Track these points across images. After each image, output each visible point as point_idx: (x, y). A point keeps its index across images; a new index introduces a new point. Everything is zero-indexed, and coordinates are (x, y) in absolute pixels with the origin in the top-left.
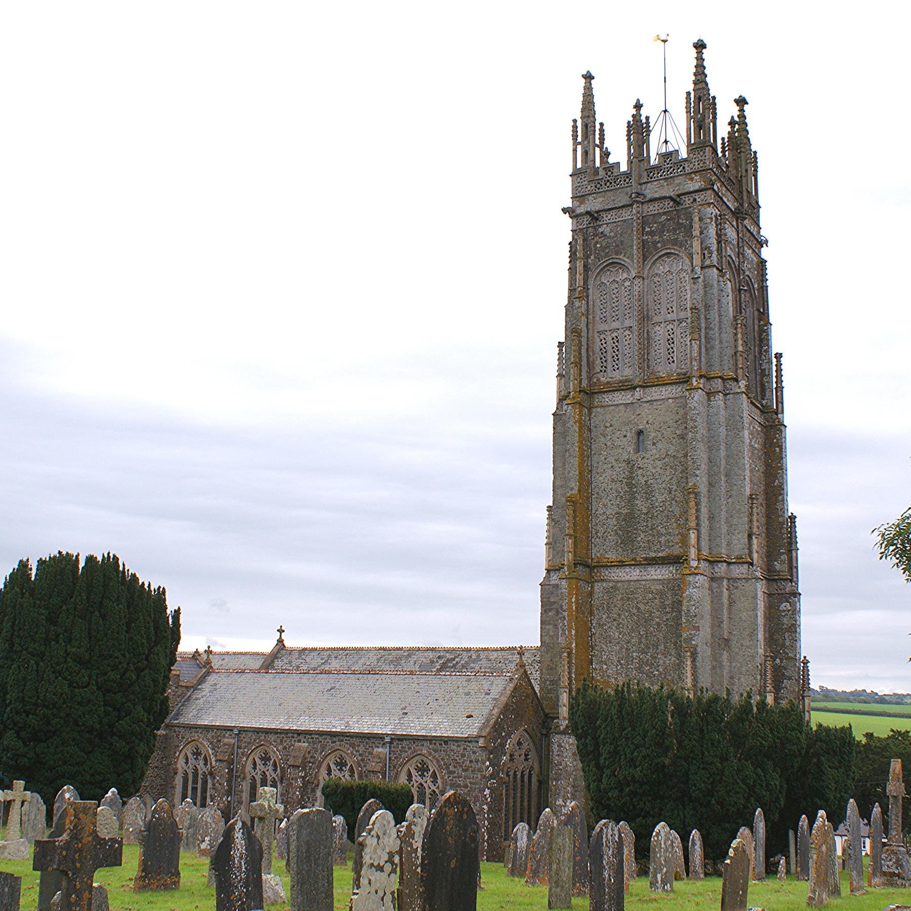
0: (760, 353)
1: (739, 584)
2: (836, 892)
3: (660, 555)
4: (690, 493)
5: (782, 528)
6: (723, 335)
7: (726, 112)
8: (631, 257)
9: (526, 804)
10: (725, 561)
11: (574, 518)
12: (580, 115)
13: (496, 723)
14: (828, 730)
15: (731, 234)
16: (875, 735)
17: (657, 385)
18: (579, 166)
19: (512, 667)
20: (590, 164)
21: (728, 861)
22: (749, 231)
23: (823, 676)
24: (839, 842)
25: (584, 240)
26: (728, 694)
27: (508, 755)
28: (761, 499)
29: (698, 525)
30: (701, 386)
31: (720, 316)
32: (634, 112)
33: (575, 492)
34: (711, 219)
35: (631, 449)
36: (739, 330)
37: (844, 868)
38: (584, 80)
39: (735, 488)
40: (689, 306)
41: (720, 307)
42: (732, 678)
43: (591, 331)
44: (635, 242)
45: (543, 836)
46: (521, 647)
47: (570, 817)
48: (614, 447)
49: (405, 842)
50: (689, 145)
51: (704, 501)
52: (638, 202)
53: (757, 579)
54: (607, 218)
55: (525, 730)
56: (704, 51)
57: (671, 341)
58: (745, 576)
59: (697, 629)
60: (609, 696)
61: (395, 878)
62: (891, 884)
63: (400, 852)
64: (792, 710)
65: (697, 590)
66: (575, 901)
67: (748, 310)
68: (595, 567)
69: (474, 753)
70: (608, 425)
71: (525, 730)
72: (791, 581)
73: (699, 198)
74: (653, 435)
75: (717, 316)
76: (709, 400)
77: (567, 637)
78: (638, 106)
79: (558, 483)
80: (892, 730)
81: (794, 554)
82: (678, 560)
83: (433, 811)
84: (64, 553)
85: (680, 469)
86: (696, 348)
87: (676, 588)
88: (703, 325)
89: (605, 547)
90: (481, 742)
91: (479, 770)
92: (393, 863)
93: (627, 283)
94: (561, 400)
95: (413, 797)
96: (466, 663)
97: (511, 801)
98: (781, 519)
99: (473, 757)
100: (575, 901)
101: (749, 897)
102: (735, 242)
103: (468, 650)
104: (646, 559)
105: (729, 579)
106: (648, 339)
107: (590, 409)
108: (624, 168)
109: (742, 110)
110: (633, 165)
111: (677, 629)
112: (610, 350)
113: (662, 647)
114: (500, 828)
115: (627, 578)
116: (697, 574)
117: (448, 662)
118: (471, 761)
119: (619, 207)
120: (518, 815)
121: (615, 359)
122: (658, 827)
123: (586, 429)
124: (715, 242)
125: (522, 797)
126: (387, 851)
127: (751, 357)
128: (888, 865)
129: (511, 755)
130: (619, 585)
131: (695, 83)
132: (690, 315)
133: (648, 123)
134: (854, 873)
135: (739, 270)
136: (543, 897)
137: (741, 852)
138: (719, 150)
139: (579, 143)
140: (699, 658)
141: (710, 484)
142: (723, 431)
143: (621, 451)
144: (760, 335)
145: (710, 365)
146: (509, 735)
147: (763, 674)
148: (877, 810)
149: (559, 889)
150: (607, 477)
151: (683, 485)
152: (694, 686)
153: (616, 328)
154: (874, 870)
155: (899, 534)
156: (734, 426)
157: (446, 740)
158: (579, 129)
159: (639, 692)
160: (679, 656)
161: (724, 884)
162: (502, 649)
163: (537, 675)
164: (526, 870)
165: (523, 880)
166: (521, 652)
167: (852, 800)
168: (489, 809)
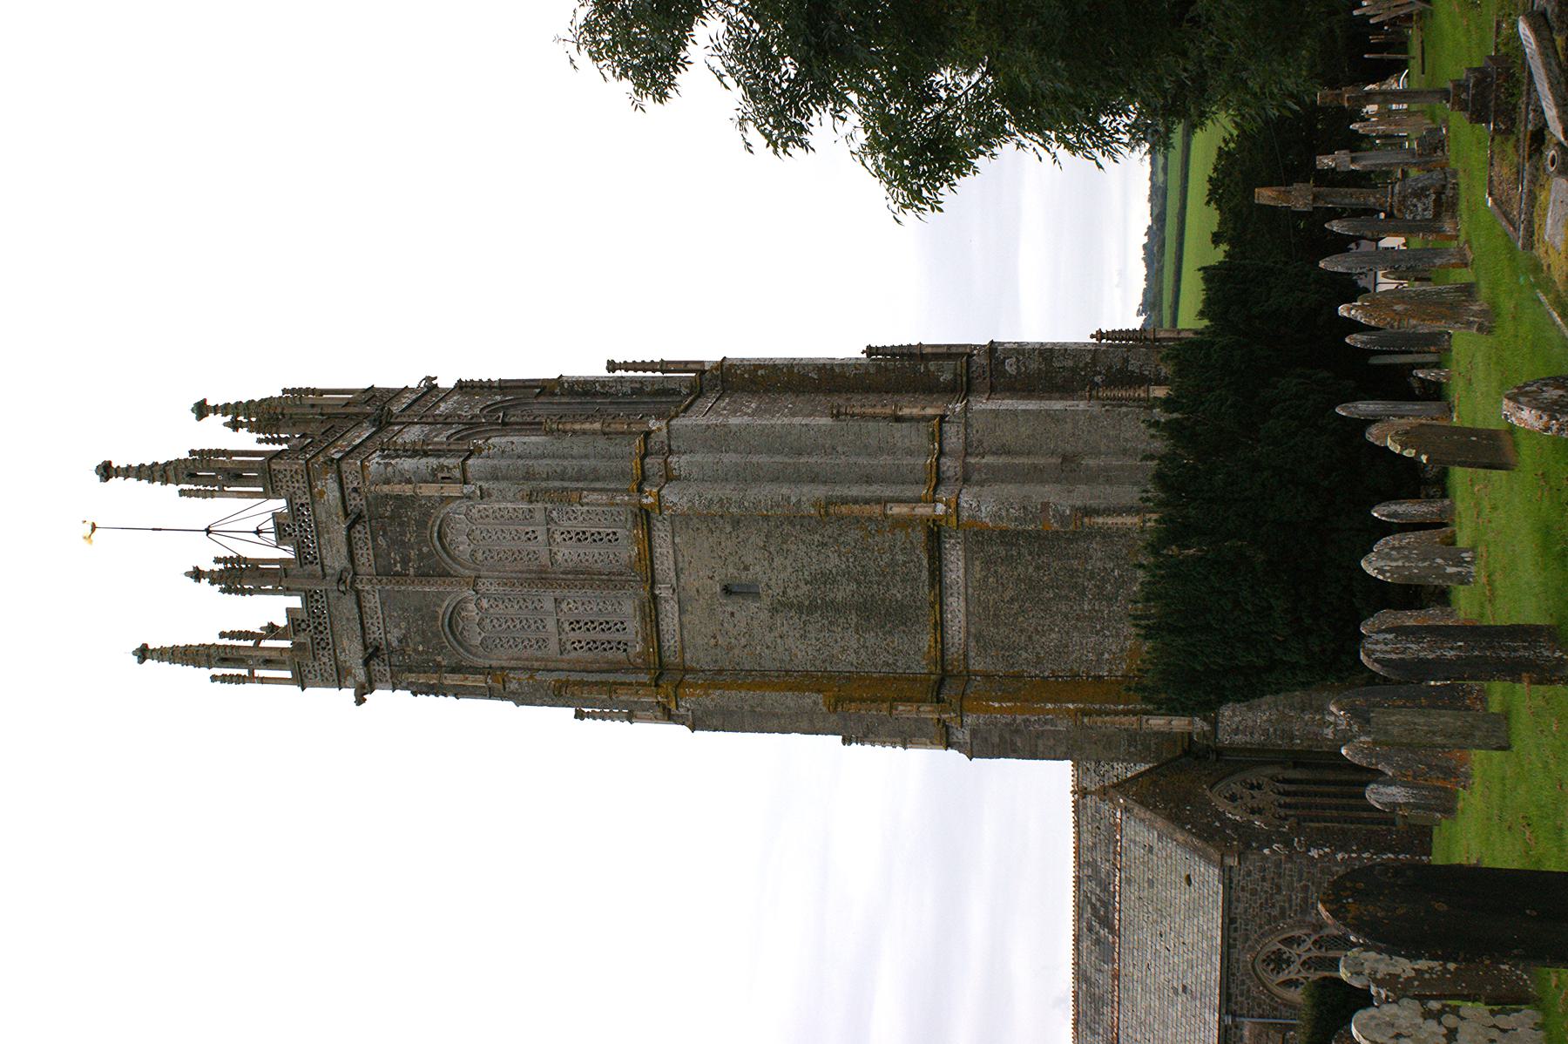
0: (605, 395)
1: (974, 436)
2: (1468, 290)
3: (925, 562)
4: (827, 513)
7: (217, 435)
8: (441, 596)
9: (1332, 789)
10: (938, 459)
11: (863, 700)
12: (204, 670)
13: (1199, 837)
14: (1208, 302)
15: (413, 434)
16: (1215, 229)
17: (652, 561)
19: (1106, 807)
20: (286, 656)
21: (1424, 458)
22: (410, 406)
23: (1123, 312)
26: (1151, 457)
27: (1252, 817)
28: (838, 400)
29: (878, 501)
31: (543, 456)
33: (820, 698)
34: (387, 465)
35: (753, 606)
36: (568, 427)
37: (1429, 280)
38: (148, 661)
39: (820, 441)
40: (525, 506)
41: (529, 456)
42: (1125, 452)
43: (560, 666)
45: (1387, 759)
46: (1074, 792)
47: (1354, 713)
48: (749, 632)
49: (1404, 989)
50: (265, 495)
51: (840, 491)
52: (353, 582)
53: (966, 409)
54: (376, 633)
55: (1211, 788)
56: (114, 465)
57: (581, 537)
59: (1045, 505)
61: (1467, 1008)
62: (1453, 206)
63: (1422, 999)
64: (1177, 357)
65: (981, 504)
66: (1495, 706)
67: (536, 412)
68: (943, 669)
69: (1249, 873)
70: (713, 642)
71: (1211, 788)
72: (970, 356)
73: (352, 482)
74: (731, 570)
75: (545, 461)
76: (678, 478)
77: (1058, 716)
78: (197, 575)
79: (805, 724)
80: (1208, 203)
81: (929, 350)
82: (935, 534)
83: (1352, 938)
84: (837, 135)
85: (787, 528)
86: (594, 497)
87: (979, 538)
88: (557, 484)
89: (912, 651)
90: (1232, 861)
91: (1278, 865)
92: (1441, 1012)
93: (485, 603)
94: (669, 717)
95: (1325, 978)
96: (1099, 884)
97: (1327, 813)
100: (1495, 706)
101: (1480, 425)
102: (427, 429)
103: (1078, 881)
104: (932, 586)
105: (967, 454)
106: (577, 573)
107: (686, 671)
108: (296, 602)
109: (216, 409)
110: (292, 586)
111: (1045, 538)
112: (592, 635)
114: (1374, 832)
115: (961, 616)
116: (958, 504)
117: (1097, 916)
118: (1264, 879)
120: (1352, 802)
121: (606, 626)
123: (719, 678)
124: (424, 460)
125: (1322, 795)
126: (1420, 1020)
127: (611, 409)
128: (1423, 209)
129: (1253, 812)
131: (166, 481)
132: (540, 505)
133: (225, 560)
134: (1438, 261)
135: (472, 425)
136: (1490, 759)
137: (1407, 438)
138: (278, 447)
139: (251, 672)
140: (1094, 503)
141: (813, 481)
142: (729, 458)
143: (755, 623)
144: (577, 394)
145: (623, 475)
146: (1219, 816)
147: (1120, 402)
148: (1336, 226)
149: (1477, 733)
150: (799, 646)
151: (813, 523)
152: (1138, 511)
153: (554, 622)
154: (1431, 232)
155: (903, 182)
156: (719, 439)
157: (1229, 921)
158: (228, 671)
159: (1148, 600)
160: (1090, 535)
161: (1463, 464)
162: (1077, 824)
163: (1119, 767)
164: (1444, 789)
165: (1462, 793)
166: (1080, 792)
167: (1322, 264)
168: (1342, 849)
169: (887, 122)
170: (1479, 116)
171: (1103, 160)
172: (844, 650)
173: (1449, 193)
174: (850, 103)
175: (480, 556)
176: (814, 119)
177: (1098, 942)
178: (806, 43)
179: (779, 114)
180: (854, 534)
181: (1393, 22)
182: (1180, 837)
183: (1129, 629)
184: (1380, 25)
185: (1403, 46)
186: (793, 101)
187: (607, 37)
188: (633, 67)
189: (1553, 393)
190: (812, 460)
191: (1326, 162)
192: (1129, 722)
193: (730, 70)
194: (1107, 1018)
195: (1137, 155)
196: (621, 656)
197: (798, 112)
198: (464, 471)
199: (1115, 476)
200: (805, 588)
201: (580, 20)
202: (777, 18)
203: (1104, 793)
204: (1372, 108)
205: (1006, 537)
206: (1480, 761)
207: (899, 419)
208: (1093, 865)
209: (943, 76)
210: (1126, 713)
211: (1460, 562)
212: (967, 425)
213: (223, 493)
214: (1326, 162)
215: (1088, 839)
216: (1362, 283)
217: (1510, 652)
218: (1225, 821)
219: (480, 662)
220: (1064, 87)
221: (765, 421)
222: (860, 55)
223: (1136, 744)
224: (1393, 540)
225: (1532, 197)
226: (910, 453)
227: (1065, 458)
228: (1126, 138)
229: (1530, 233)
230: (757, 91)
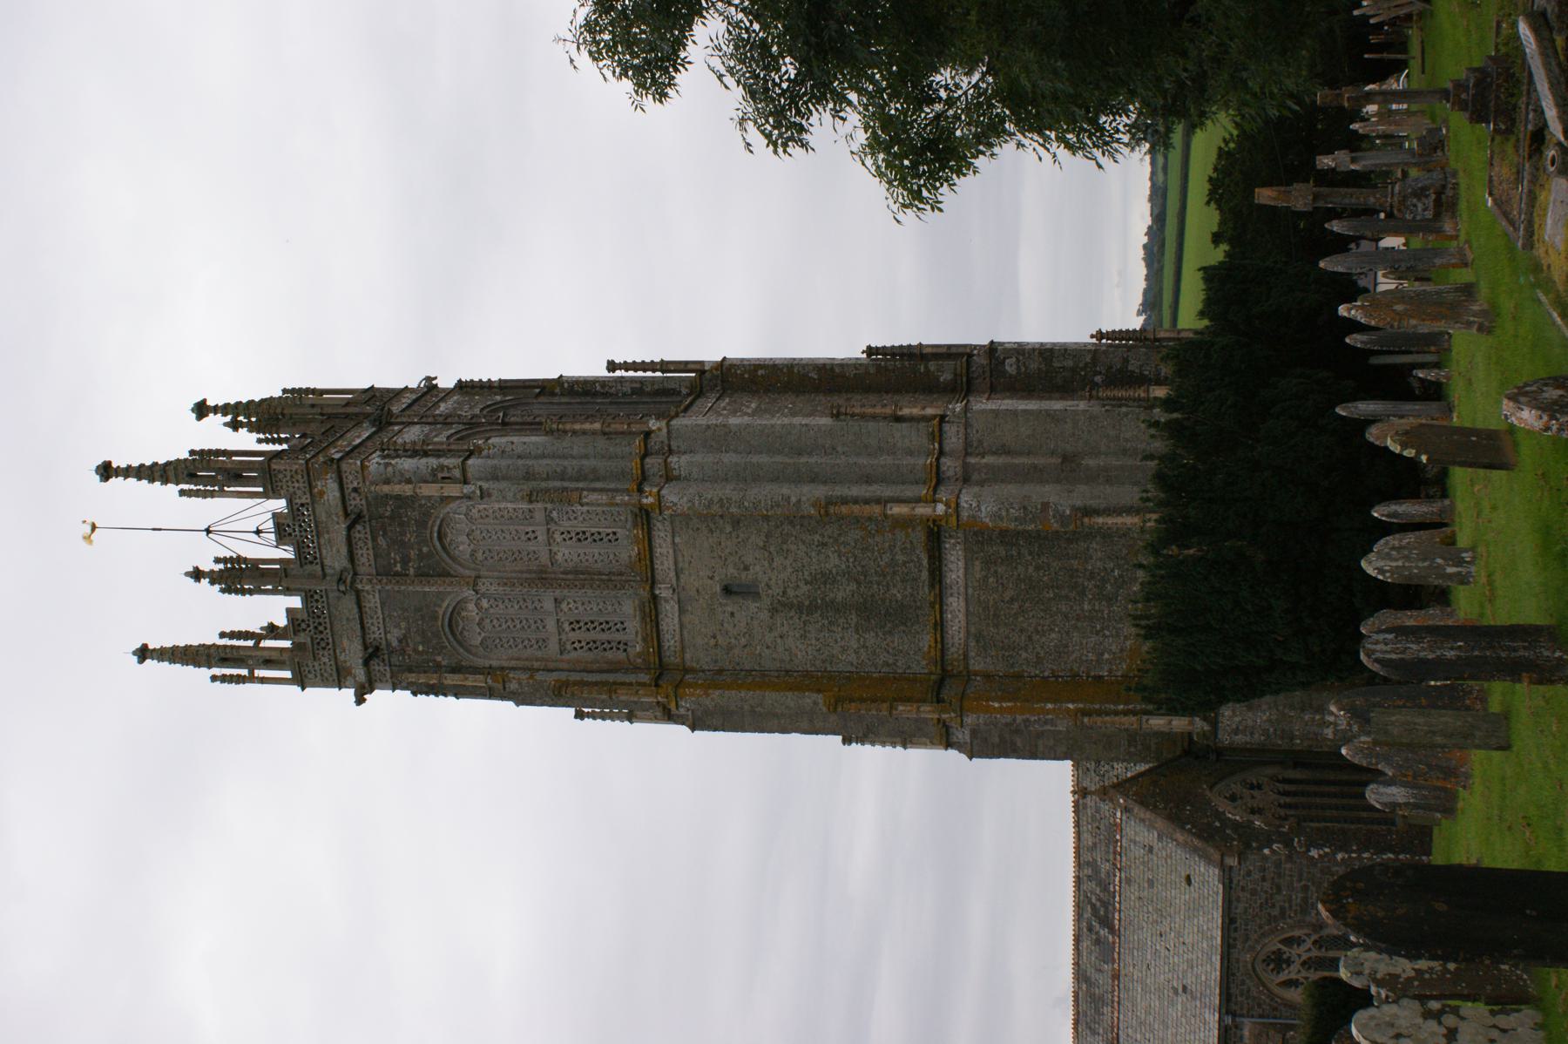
0: (605, 395)
2: (1468, 290)
4: (827, 514)
5: (886, 369)
6: (575, 452)
7: (217, 435)
8: (441, 596)
9: (1332, 789)
10: (938, 459)
11: (862, 700)
12: (203, 670)
13: (1199, 836)
14: (1208, 302)
15: (413, 434)
17: (652, 562)
19: (1105, 807)
20: (285, 656)
21: (1424, 458)
22: (410, 406)
23: (1123, 312)
24: (1386, 284)
25: (410, 670)
26: (1150, 457)
27: (1252, 817)
28: (838, 400)
29: (878, 501)
30: (655, 490)
31: (543, 456)
32: (205, 582)
33: (820, 698)
34: (387, 465)
36: (568, 427)
37: (1428, 279)
38: (148, 661)
40: (525, 506)
42: (1125, 452)
43: (561, 666)
44: (418, 589)
46: (1074, 792)
47: (1360, 716)
50: (266, 495)
51: (840, 491)
52: (353, 581)
53: (966, 409)
54: (376, 633)
55: (1211, 788)
56: (114, 465)
57: (581, 537)
58: (962, 430)
59: (1045, 506)
60: (1155, 650)
61: (1467, 1008)
63: (1422, 999)
64: (1177, 356)
65: (981, 504)
66: (1495, 706)
67: (536, 412)
68: (943, 669)
69: (1249, 873)
70: (712, 642)
71: (1211, 788)
72: (970, 356)
73: (352, 482)
75: (545, 462)
76: (678, 478)
78: (197, 575)
82: (935, 535)
83: (1352, 938)
84: (838, 134)
85: (787, 528)
86: (593, 497)
87: (978, 537)
88: (558, 484)
89: (912, 651)
90: (1232, 861)
91: (1278, 865)
93: (485, 603)
94: (669, 716)
95: (1325, 978)
97: (1328, 813)
98: (872, 370)
99: (1257, 876)
100: (1495, 706)
101: (1480, 425)
102: (427, 429)
103: (1078, 881)
104: (932, 586)
106: (576, 572)
107: (687, 671)
108: (296, 602)
109: (216, 410)
110: (292, 586)
112: (593, 635)
113: (1075, 563)
115: (961, 616)
116: (958, 504)
117: (1097, 916)
118: (1264, 879)
119: (360, 607)
120: (1352, 802)
121: (606, 626)
122: (1371, 571)
123: (719, 678)
124: (424, 460)
126: (1420, 1020)
128: (1423, 209)
129: (1253, 812)
130: (973, 630)
131: (165, 481)
132: (540, 505)
133: (224, 560)
134: (1438, 261)
135: (472, 425)
137: (1407, 438)
138: (278, 447)
139: (251, 672)
140: (1093, 503)
141: (813, 481)
142: (729, 458)
143: (755, 622)
144: (577, 394)
146: (1219, 815)
147: (1120, 402)
148: (1336, 226)
149: (1477, 733)
150: (798, 646)
154: (1431, 232)
155: (903, 182)
156: (720, 439)
157: (1229, 922)
158: (228, 671)
159: (1148, 600)
160: (1090, 535)
162: (1077, 824)
163: (1119, 768)
164: (1444, 789)
165: (1462, 793)
166: (1081, 792)
167: (1322, 264)
168: (1341, 849)
169: (887, 122)
170: (1478, 116)
171: (1103, 161)
173: (1450, 193)
174: (850, 103)
175: (480, 556)
176: (814, 119)
177: (1098, 942)
178: (806, 43)
179: (779, 114)
180: (855, 534)
181: (1393, 22)
182: (1180, 837)
183: (1129, 629)
184: (1380, 25)
185: (1403, 46)
187: (607, 37)
188: (633, 67)
189: (1553, 393)
190: (812, 460)
191: (1326, 162)
192: (1129, 721)
193: (730, 70)
194: (1107, 1018)
196: (621, 656)
198: (464, 471)
199: (1115, 476)
200: (805, 588)
201: (580, 19)
203: (1104, 793)
204: (1372, 108)
206: (1479, 761)
207: (899, 419)
208: (1093, 864)
209: (943, 76)
210: (1125, 713)
211: (1460, 562)
212: (967, 425)
213: (222, 494)
214: (1326, 162)
215: (1088, 839)
216: (1362, 283)
217: (1510, 652)
218: (1226, 822)
221: (765, 421)
223: (1136, 744)
224: (1393, 540)
225: (1532, 198)
226: (910, 453)
227: (1065, 458)
228: (1126, 138)
229: (1530, 233)
230: (757, 92)
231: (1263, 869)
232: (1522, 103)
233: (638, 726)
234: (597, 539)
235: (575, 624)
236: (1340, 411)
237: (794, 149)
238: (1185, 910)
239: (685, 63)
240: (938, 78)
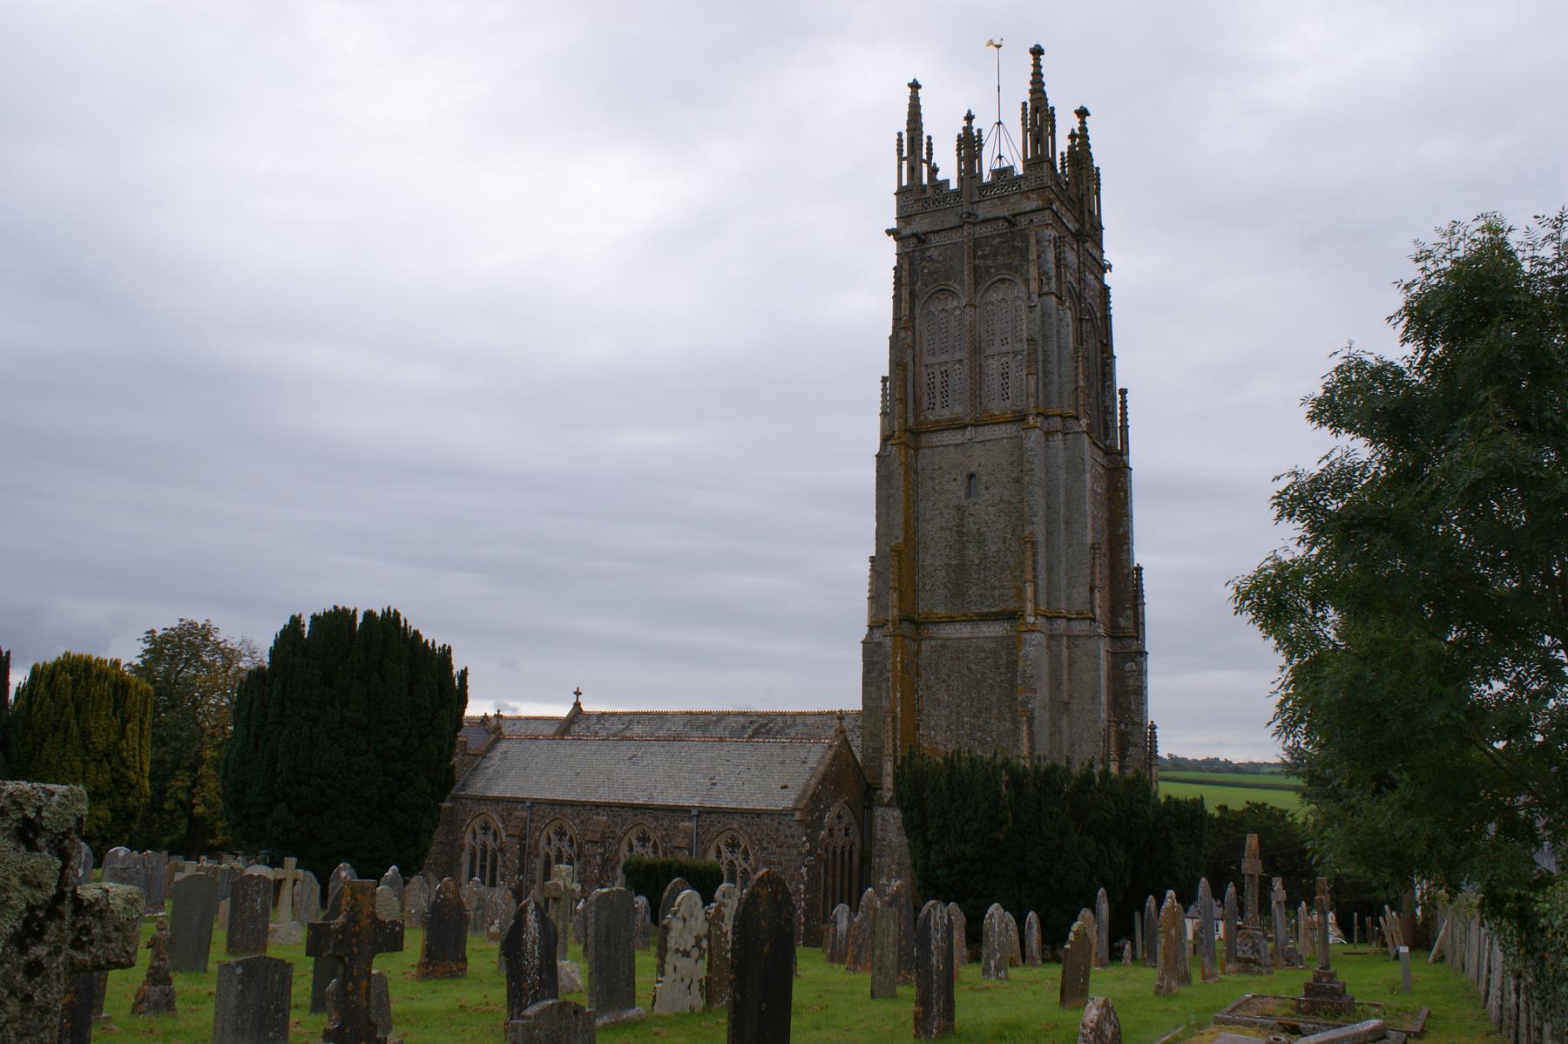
0: (1103, 388)
2: (1186, 979)
7: (1065, 124)
13: (814, 794)
14: (1177, 802)
15: (1071, 258)
16: (503, 689)
18: (905, 183)
19: (832, 732)
23: (1168, 746)
24: (1190, 926)
26: (1068, 762)
28: (1104, 548)
29: (1035, 577)
32: (965, 124)
33: (900, 541)
35: (962, 494)
40: (1025, 336)
41: (1059, 338)
42: (1072, 745)
47: (895, 898)
50: (1025, 160)
51: (1042, 550)
53: (1099, 636)
54: (935, 240)
57: (1005, 376)
59: (1034, 691)
61: (703, 964)
62: (1246, 971)
63: (709, 936)
65: (1034, 648)
66: (900, 989)
73: (1036, 218)
78: (969, 118)
82: (1013, 616)
84: (1287, 541)
86: (1032, 383)
87: (1011, 646)
88: (1041, 358)
89: (933, 602)
90: (797, 815)
91: (795, 846)
93: (958, 312)
94: (885, 440)
99: (788, 832)
100: (900, 989)
101: (1091, 985)
103: (783, 714)
104: (978, 614)
106: (981, 373)
108: (954, 185)
109: (1083, 122)
112: (938, 385)
113: (995, 711)
121: (944, 395)
123: (912, 472)
128: (1244, 951)
131: (1032, 92)
133: (980, 135)
134: (1206, 959)
135: (1079, 298)
137: (1082, 936)
138: (1058, 166)
140: (1036, 723)
142: (1062, 474)
146: (828, 808)
147: (1107, 741)
148: (1231, 890)
150: (936, 525)
152: (1031, 753)
155: (1255, 587)
157: (758, 814)
158: (905, 143)
160: (1014, 721)
161: (1064, 972)
162: (820, 714)
163: (858, 742)
165: (843, 967)
166: (841, 716)
169: (1298, 575)
170: (1309, 989)
171: (1273, 726)
172: (933, 556)
173: (1256, 969)
174: (1311, 549)
175: (990, 308)
176: (1299, 524)
177: (743, 727)
178: (1353, 518)
179: (1301, 499)
180: (1012, 561)
181: (1381, 933)
182: (813, 782)
183: (951, 747)
184: (1378, 924)
185: (1364, 940)
186: (1310, 509)
187: (1354, 377)
188: (1332, 397)
189: (1109, 1030)
190: (1062, 531)
191: (1277, 883)
192: (889, 749)
193: (1332, 464)
194: (694, 734)
195: (1281, 752)
196: (925, 406)
197: (1302, 513)
198: (1047, 294)
199: (1062, 739)
200: (974, 528)
201: (1366, 358)
202: (1371, 497)
203: (842, 731)
204: (1315, 918)
205: (1012, 664)
206: (864, 979)
207: (1092, 590)
208: (794, 724)
209: (1332, 614)
210: (895, 746)
211: (998, 969)
212: (1089, 637)
213: (1025, 131)
214: (1277, 883)
215: (810, 721)
216: (1192, 908)
217: (936, 1004)
218: (824, 811)
219: (918, 311)
220: (1325, 698)
221: (1088, 499)
222: (1346, 556)
223: (874, 754)
224: (1013, 924)
225: (1251, 1025)
226: (1069, 598)
227: (1067, 704)
228: (1290, 743)
229: (1225, 1022)
230: (1317, 484)
231: (793, 836)
232: (1320, 1020)
233: (878, 419)
234: (1005, 386)
235: (945, 374)
236: (1102, 890)
237: (1276, 511)
238: (769, 785)
239: (1337, 433)
240: (1331, 611)
